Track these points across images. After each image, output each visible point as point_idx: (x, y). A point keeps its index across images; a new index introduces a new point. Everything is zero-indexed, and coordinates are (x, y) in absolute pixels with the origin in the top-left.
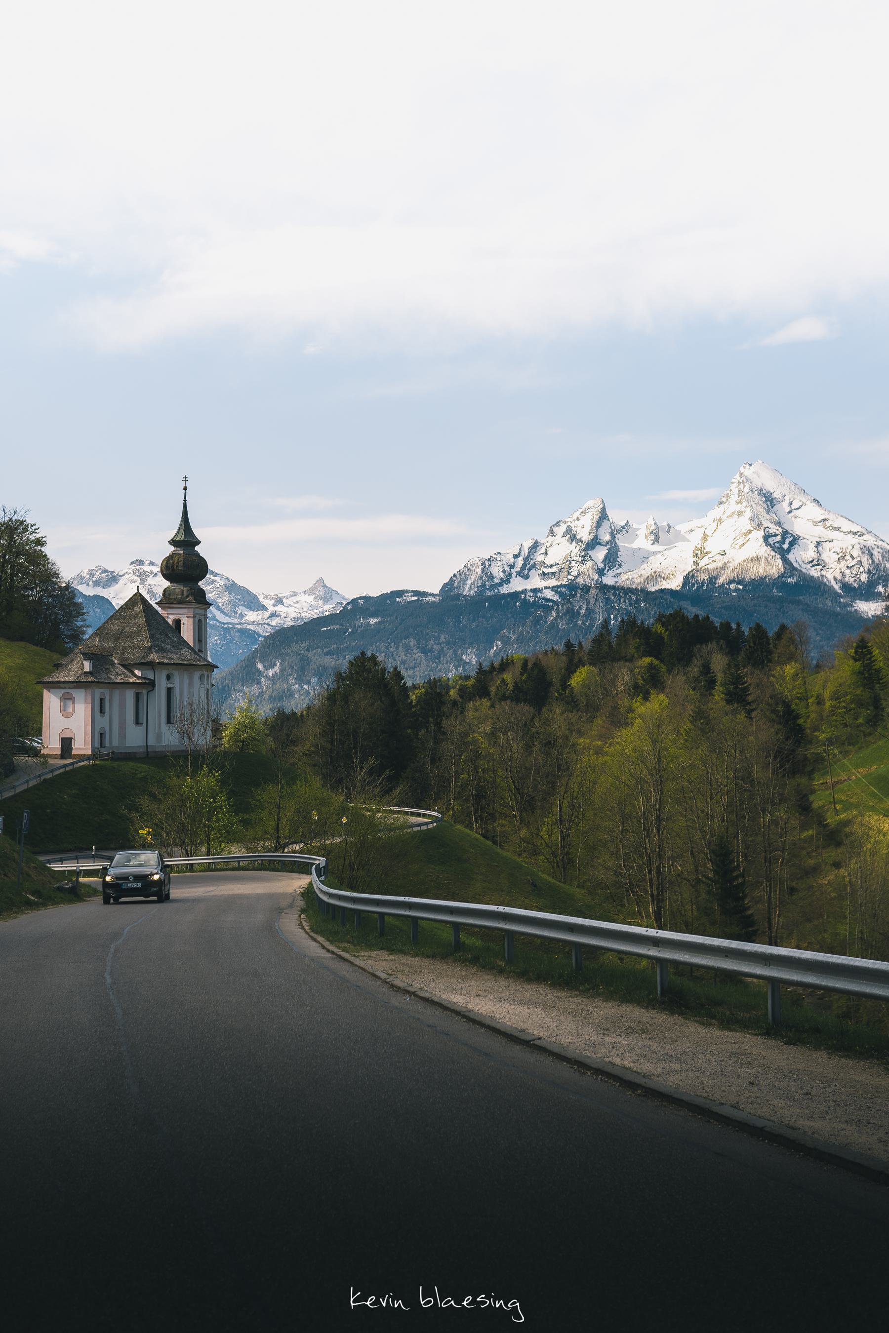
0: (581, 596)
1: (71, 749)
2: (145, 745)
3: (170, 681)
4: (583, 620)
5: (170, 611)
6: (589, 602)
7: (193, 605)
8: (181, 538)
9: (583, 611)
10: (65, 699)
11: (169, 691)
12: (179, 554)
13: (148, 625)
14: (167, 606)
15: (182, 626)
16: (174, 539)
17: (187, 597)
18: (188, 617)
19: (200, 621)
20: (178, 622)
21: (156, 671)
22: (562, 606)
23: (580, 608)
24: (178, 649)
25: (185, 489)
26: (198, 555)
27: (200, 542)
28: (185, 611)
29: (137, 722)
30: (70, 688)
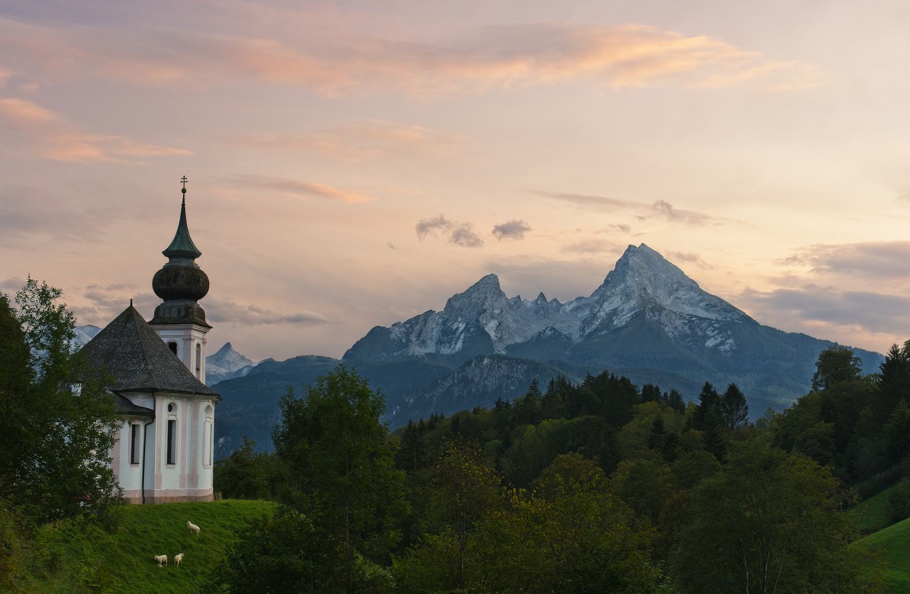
0: (476, 365)
2: (141, 489)
3: (172, 413)
11: (171, 424)
22: (458, 375)
25: (184, 191)
27: (200, 254)
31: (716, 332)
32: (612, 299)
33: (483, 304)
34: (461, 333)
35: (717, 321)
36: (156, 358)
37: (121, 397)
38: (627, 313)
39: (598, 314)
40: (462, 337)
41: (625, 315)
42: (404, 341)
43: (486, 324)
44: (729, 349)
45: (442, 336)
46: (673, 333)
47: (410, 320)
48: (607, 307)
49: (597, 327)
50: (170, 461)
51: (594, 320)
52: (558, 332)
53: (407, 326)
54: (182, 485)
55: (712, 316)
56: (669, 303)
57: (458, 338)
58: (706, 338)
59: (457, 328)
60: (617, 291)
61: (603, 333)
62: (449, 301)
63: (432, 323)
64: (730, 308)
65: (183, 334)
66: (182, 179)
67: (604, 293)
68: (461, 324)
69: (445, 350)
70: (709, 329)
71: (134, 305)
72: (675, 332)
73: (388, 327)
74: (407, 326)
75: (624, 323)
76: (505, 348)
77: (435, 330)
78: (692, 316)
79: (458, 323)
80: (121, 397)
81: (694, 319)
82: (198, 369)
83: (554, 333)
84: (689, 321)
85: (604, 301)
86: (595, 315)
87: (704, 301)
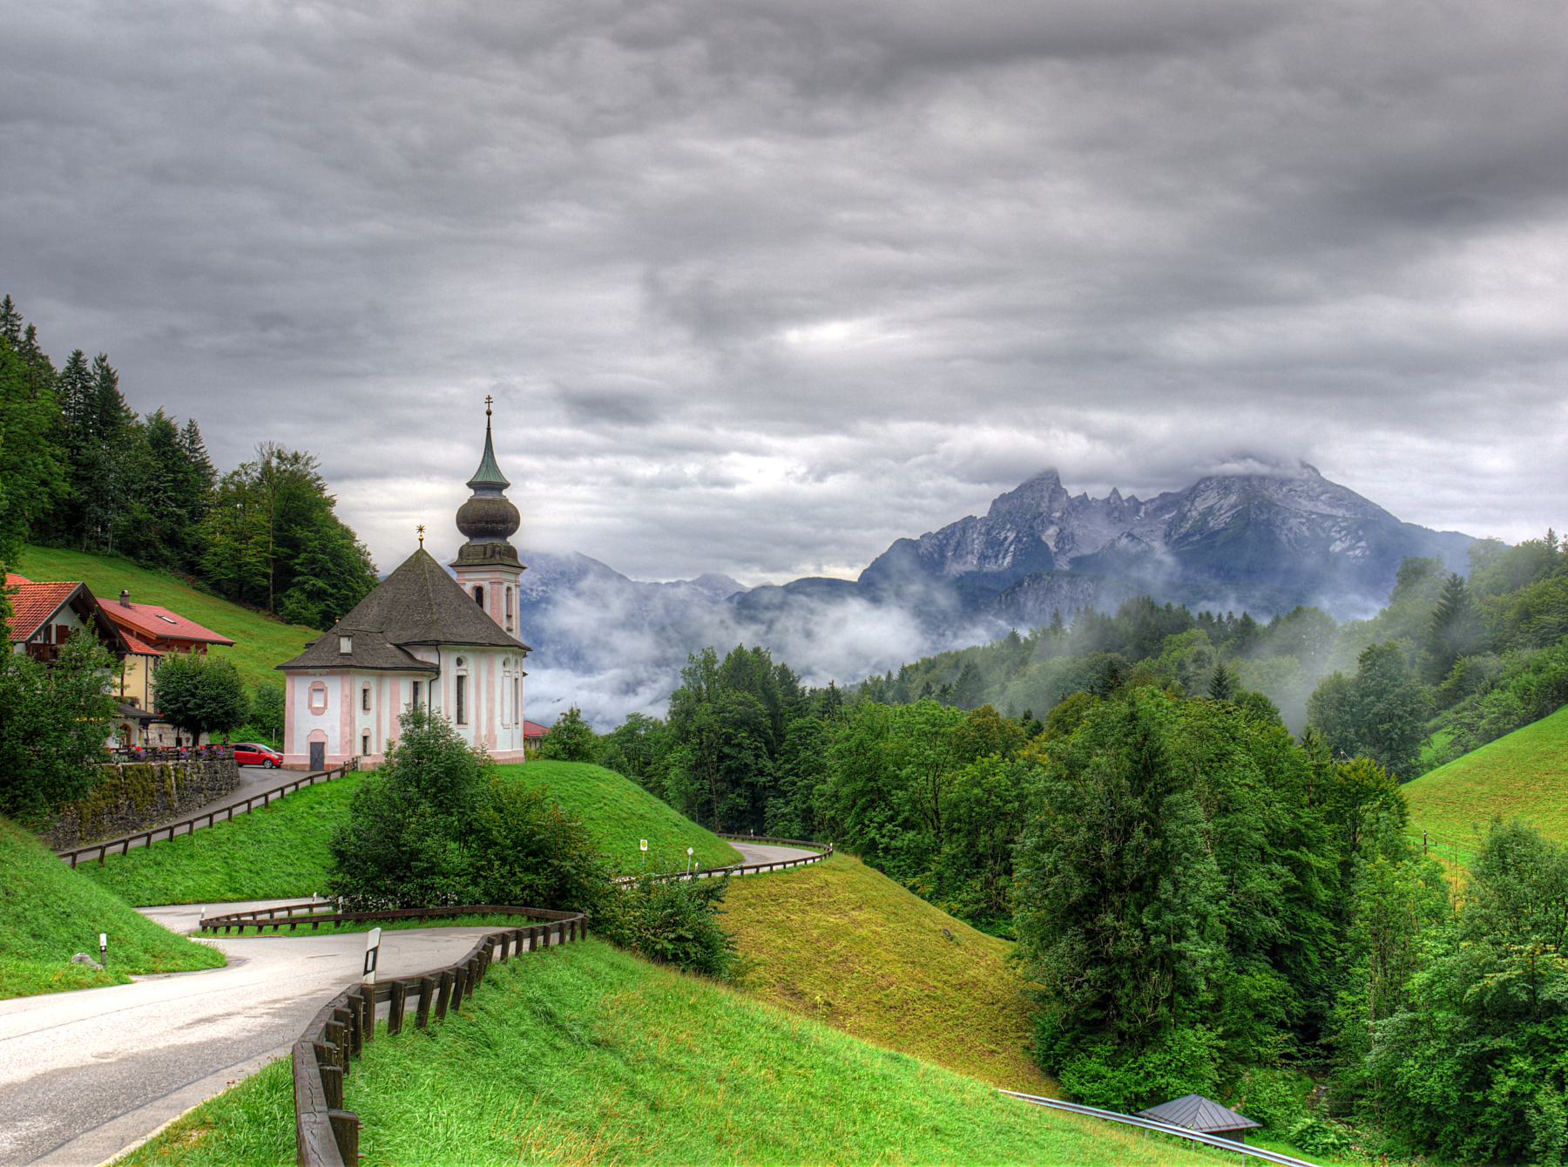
1: (323, 758)
3: (463, 667)
5: (468, 576)
10: (315, 690)
11: (460, 679)
14: (464, 569)
20: (479, 591)
25: (489, 413)
27: (509, 485)
29: (365, 708)
30: (321, 675)
31: (1343, 533)
32: (1207, 494)
33: (1038, 505)
34: (1011, 544)
35: (1345, 519)
37: (403, 650)
38: (1226, 512)
40: (1012, 549)
42: (936, 556)
43: (1043, 532)
47: (943, 529)
48: (1201, 505)
51: (1182, 521)
53: (941, 537)
56: (1280, 496)
57: (1007, 551)
61: (1195, 539)
62: (995, 502)
63: (973, 533)
69: (991, 567)
71: (424, 547)
77: (976, 542)
78: (1312, 513)
80: (403, 650)
81: (1314, 516)
82: (509, 617)
84: (1308, 520)
85: (1196, 497)
86: (1185, 515)
87: (1327, 492)
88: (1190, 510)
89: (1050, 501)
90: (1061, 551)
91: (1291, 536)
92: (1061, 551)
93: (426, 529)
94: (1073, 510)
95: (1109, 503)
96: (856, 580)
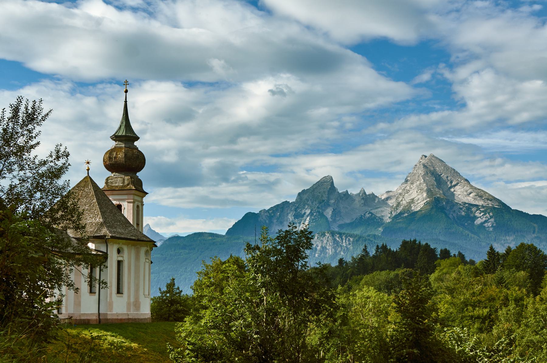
0: (318, 238)
2: (97, 312)
3: (121, 254)
4: (319, 254)
6: (323, 242)
7: (134, 192)
8: (122, 133)
9: (319, 248)
11: (119, 263)
12: (121, 148)
13: (99, 204)
15: (123, 210)
16: (117, 134)
17: (128, 185)
18: (128, 202)
19: (138, 206)
21: (108, 244)
23: (317, 246)
24: (126, 226)
26: (136, 148)
28: (125, 197)
31: (482, 214)
35: (483, 206)
36: (108, 214)
39: (401, 202)
41: (419, 203)
44: (490, 226)
45: (294, 219)
46: (452, 215)
48: (408, 198)
49: (401, 212)
50: (119, 291)
52: (374, 215)
54: (128, 309)
55: (481, 203)
58: (476, 218)
59: (305, 213)
60: (329, 247)
61: (405, 215)
64: (491, 198)
65: (127, 198)
66: (125, 82)
67: (405, 188)
68: (307, 210)
70: (478, 212)
72: (454, 215)
73: (256, 213)
74: (270, 212)
75: (419, 209)
76: (338, 227)
79: (305, 210)
81: (467, 205)
83: (371, 216)
88: (402, 200)
89: (328, 194)
90: (334, 221)
91: (455, 215)
92: (334, 221)
93: (92, 162)
94: (341, 199)
95: (359, 196)
96: (224, 234)
